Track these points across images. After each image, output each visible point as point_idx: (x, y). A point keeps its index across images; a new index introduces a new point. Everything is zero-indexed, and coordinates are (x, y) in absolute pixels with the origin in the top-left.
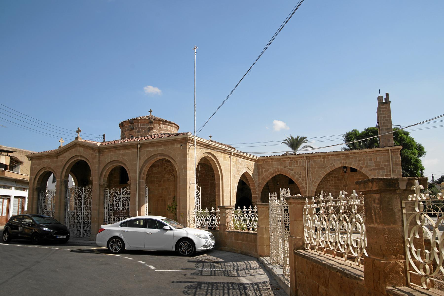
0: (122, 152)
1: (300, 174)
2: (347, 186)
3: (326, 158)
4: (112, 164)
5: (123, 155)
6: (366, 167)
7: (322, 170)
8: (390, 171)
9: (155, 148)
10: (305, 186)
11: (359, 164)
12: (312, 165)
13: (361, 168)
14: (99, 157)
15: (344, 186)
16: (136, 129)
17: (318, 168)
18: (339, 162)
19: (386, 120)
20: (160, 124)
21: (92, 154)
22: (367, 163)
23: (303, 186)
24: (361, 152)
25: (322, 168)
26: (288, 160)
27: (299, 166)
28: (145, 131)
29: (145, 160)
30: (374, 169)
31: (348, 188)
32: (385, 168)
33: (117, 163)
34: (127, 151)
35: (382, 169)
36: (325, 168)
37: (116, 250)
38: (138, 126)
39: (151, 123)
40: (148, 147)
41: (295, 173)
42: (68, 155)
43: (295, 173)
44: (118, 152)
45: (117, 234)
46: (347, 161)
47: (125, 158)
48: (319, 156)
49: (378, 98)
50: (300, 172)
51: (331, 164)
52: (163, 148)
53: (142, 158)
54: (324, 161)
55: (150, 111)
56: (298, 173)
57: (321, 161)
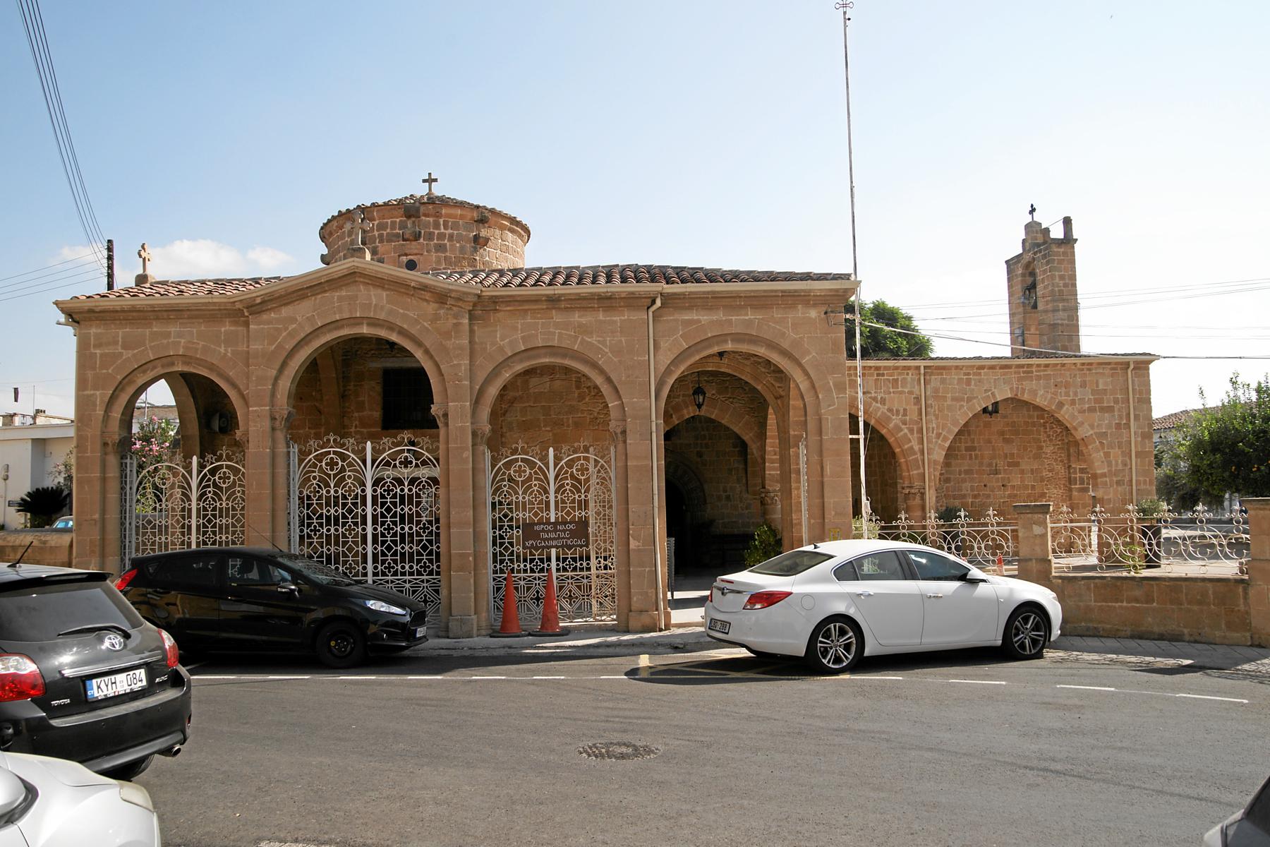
0: (576, 318)
1: (905, 415)
2: (974, 449)
3: (975, 374)
4: (529, 358)
5: (584, 329)
6: (1073, 403)
7: (962, 406)
8: (1129, 414)
9: (720, 315)
10: (916, 448)
11: (1055, 394)
12: (936, 390)
13: (1061, 405)
14: (472, 332)
15: (967, 449)
16: (430, 237)
17: (953, 399)
18: (1007, 388)
19: (1065, 285)
20: (502, 228)
21: (436, 318)
22: (1076, 394)
23: (912, 448)
24: (1063, 365)
25: (962, 400)
26: (872, 375)
27: (901, 393)
28: (462, 249)
29: (676, 352)
30: (1092, 410)
31: (976, 456)
32: (1116, 407)
33: (554, 355)
34: (601, 316)
35: (1110, 409)
36: (969, 400)
37: (838, 660)
38: (437, 226)
39: (482, 221)
40: (690, 308)
41: (890, 410)
42: (304, 315)
43: (890, 410)
44: (558, 317)
45: (840, 608)
46: (1027, 385)
47: (593, 340)
48: (957, 367)
49: (1027, 226)
50: (905, 410)
51: (986, 391)
52: (750, 315)
53: (664, 345)
54: (968, 382)
55: (430, 180)
56: (898, 411)
57: (960, 380)
